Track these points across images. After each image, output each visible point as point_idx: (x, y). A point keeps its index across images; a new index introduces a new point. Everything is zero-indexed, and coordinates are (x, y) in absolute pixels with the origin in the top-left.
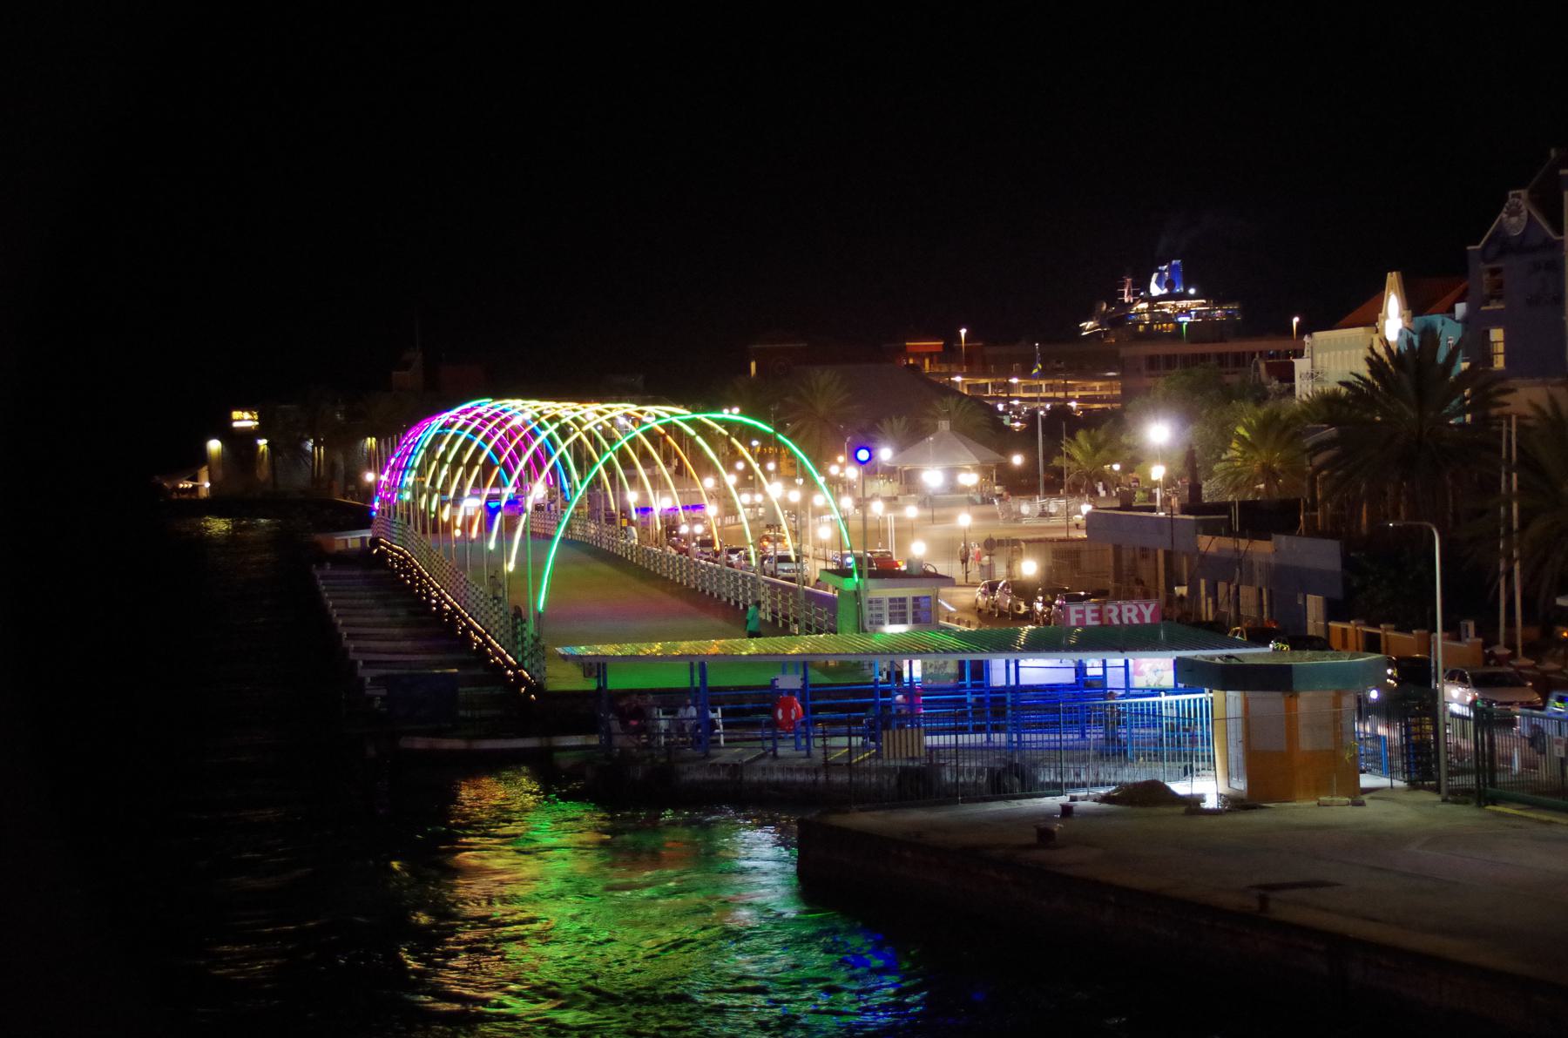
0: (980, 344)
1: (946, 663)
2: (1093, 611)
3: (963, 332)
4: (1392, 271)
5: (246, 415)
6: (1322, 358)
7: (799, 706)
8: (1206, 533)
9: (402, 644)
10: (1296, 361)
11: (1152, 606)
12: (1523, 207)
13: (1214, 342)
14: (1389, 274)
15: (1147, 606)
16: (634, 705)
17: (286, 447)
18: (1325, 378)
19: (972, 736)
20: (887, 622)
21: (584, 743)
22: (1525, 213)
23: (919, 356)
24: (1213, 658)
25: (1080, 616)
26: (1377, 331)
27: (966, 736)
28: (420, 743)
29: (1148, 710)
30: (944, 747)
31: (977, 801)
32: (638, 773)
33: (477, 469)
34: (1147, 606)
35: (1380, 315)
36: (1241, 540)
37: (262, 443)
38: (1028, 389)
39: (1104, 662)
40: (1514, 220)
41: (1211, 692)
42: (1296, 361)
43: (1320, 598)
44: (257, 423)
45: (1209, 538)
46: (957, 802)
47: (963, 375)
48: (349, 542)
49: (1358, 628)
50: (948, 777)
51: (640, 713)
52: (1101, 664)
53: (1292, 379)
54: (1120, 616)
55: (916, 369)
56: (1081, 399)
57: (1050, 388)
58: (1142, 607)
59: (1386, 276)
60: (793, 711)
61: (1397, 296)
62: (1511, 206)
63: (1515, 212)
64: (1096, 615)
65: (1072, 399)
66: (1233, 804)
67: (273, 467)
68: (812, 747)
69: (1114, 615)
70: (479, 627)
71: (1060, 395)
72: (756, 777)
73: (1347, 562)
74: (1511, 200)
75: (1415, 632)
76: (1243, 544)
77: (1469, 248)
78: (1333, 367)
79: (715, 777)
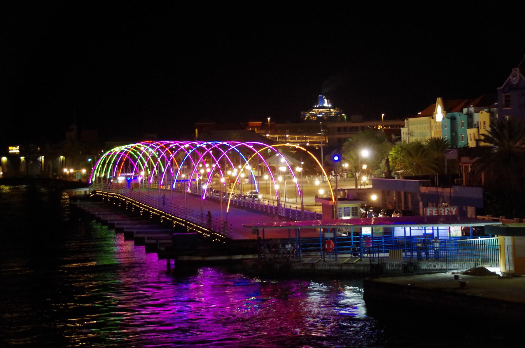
0: (274, 123)
1: (379, 229)
2: (435, 210)
3: (269, 119)
4: (438, 97)
5: (14, 148)
6: (412, 127)
7: (333, 243)
8: (423, 186)
9: (137, 226)
10: (402, 129)
11: (455, 209)
12: (518, 74)
13: (360, 122)
14: (438, 98)
15: (454, 209)
16: (274, 243)
17: (32, 157)
18: (413, 135)
19: (384, 254)
20: (343, 216)
21: (242, 258)
22: (518, 76)
23: (253, 127)
24: (498, 225)
25: (431, 212)
26: (433, 118)
27: (382, 254)
28: (186, 258)
29: (473, 243)
30: (385, 257)
31: (399, 276)
32: (278, 266)
33: (111, 165)
34: (454, 209)
35: (434, 112)
36: (439, 188)
37: (22, 158)
38: (291, 139)
39: (438, 228)
40: (514, 79)
41: (497, 237)
42: (402, 129)
43: (473, 208)
44: (18, 151)
45: (425, 188)
46: (413, 275)
47: (270, 134)
48: (77, 193)
49: (490, 218)
50: (388, 267)
51: (276, 246)
52: (432, 229)
53: (401, 135)
54: (444, 212)
55: (253, 131)
56: (310, 142)
57: (298, 138)
58: (452, 209)
59: (436, 99)
60: (331, 245)
61: (441, 106)
62: (513, 73)
63: (514, 76)
64: (436, 212)
65: (307, 142)
66: (508, 275)
67: (27, 167)
68: (337, 258)
69: (442, 211)
70: (180, 219)
71: (304, 141)
72: (320, 268)
73: (484, 194)
74: (513, 72)
75: (515, 219)
76: (440, 190)
77: (498, 88)
78: (416, 131)
79: (305, 268)
